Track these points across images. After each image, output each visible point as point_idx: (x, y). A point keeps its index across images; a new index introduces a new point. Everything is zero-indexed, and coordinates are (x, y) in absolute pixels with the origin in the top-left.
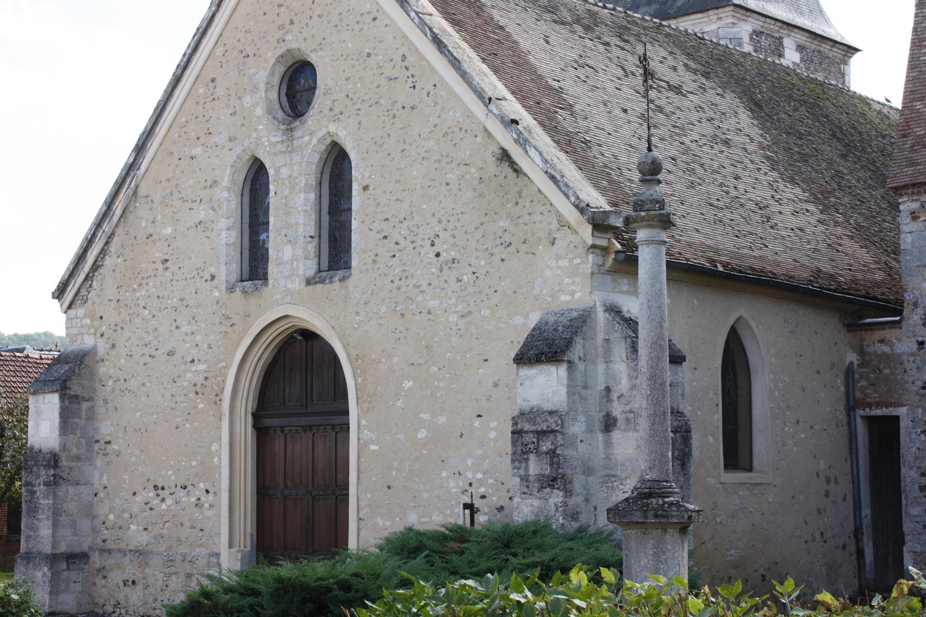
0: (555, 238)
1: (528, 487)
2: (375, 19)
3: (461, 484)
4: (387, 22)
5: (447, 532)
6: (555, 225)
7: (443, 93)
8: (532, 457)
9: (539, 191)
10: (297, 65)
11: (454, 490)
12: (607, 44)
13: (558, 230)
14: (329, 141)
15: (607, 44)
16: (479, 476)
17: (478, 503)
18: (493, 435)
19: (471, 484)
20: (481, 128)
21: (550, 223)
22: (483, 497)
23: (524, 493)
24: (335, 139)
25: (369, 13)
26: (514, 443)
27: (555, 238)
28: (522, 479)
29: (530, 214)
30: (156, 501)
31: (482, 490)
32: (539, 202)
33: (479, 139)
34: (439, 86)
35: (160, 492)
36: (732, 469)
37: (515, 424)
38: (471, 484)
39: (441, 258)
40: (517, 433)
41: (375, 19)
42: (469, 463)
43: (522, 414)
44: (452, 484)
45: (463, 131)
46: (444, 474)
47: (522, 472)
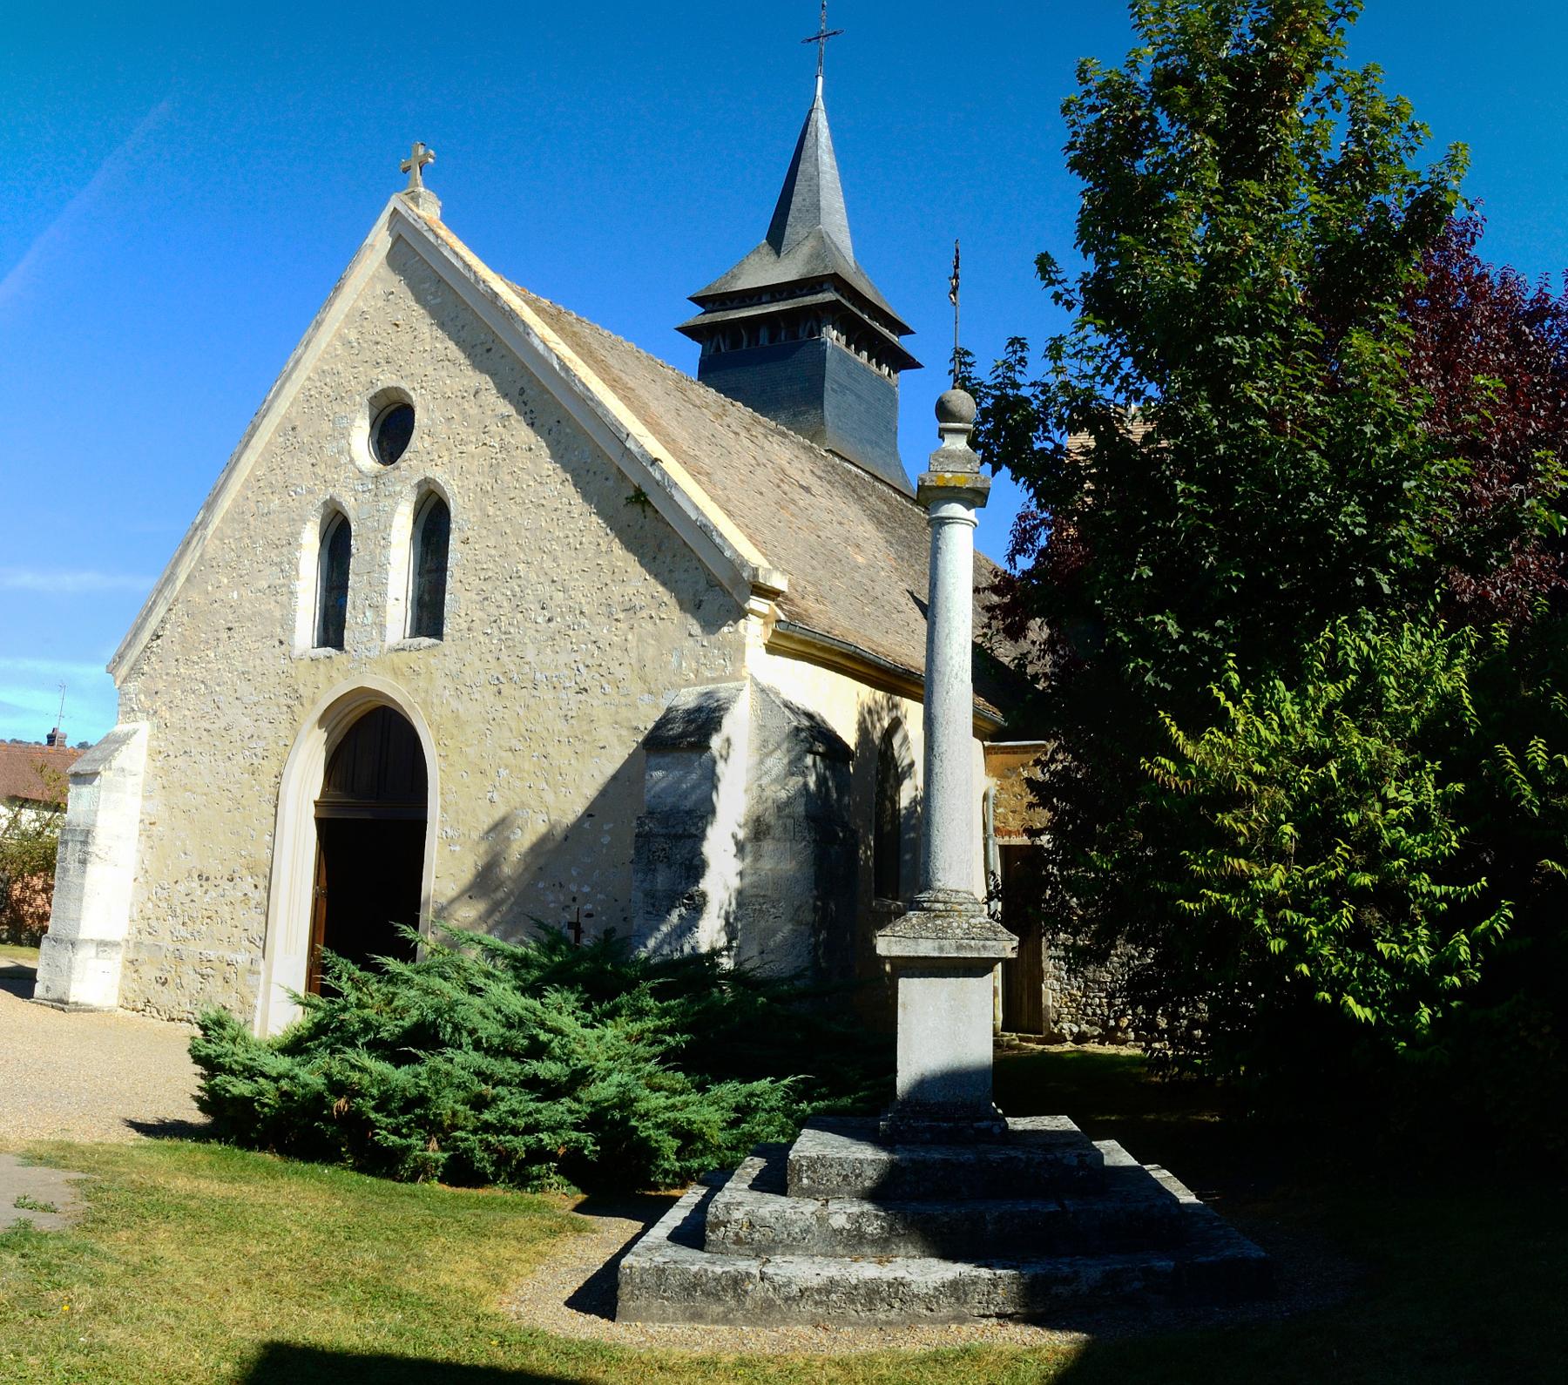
0: (701, 601)
1: (654, 906)
2: (489, 350)
3: (562, 898)
4: (504, 352)
5: (557, 367)
6: (702, 584)
7: (568, 430)
8: (660, 867)
9: (685, 543)
10: (392, 408)
11: (552, 905)
12: (736, 433)
13: (707, 590)
14: (425, 488)
15: (736, 433)
16: (586, 889)
17: (584, 922)
18: (606, 840)
19: (574, 899)
20: (614, 470)
21: (697, 583)
22: (589, 915)
23: (648, 913)
24: (432, 487)
25: (482, 344)
26: (638, 850)
27: (701, 601)
28: (646, 895)
29: (671, 571)
30: (199, 892)
31: (589, 906)
32: (684, 556)
33: (610, 483)
34: (563, 422)
35: (204, 883)
36: (420, 585)
37: (641, 825)
38: (574, 899)
39: (552, 625)
40: (643, 839)
41: (489, 350)
42: (574, 873)
43: (651, 813)
44: (551, 897)
45: (591, 473)
46: (541, 885)
47: (646, 885)
